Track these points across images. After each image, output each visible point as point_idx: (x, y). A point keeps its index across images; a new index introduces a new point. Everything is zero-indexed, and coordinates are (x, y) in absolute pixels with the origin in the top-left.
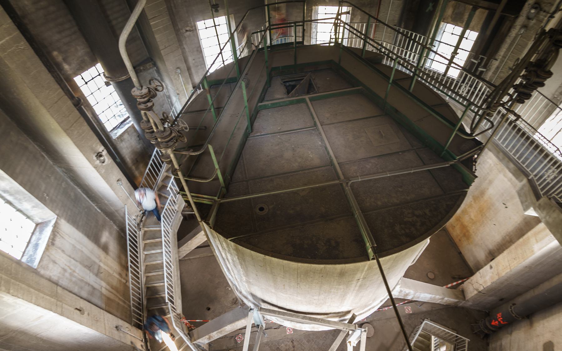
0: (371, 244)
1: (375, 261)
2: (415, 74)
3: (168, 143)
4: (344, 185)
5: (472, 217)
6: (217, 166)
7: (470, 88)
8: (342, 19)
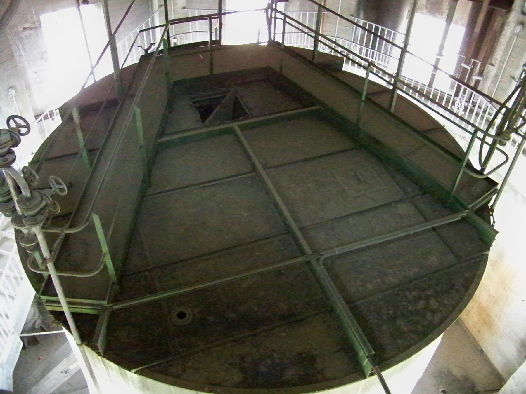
0: (366, 352)
1: (376, 377)
2: (394, 85)
3: (36, 217)
4: (314, 263)
5: (493, 293)
6: (105, 249)
7: (466, 104)
8: (278, 9)
